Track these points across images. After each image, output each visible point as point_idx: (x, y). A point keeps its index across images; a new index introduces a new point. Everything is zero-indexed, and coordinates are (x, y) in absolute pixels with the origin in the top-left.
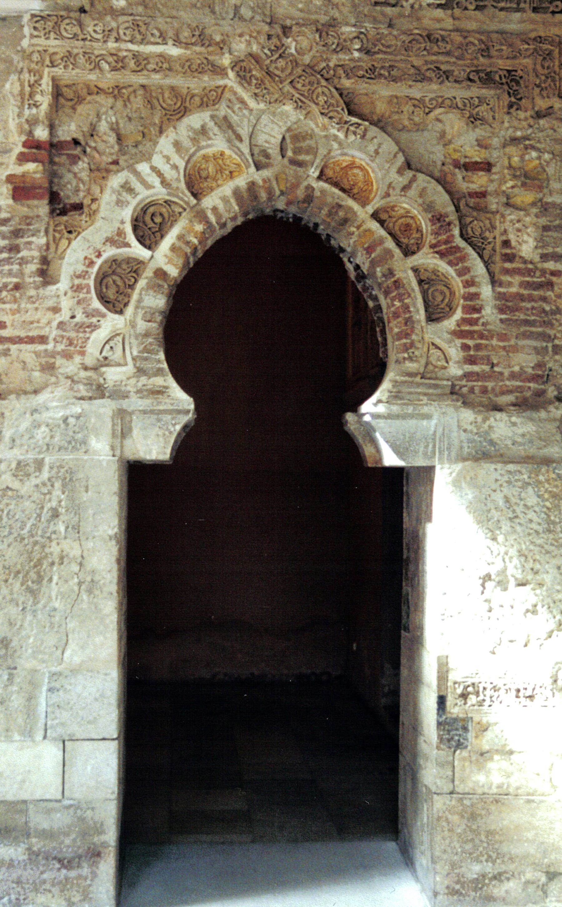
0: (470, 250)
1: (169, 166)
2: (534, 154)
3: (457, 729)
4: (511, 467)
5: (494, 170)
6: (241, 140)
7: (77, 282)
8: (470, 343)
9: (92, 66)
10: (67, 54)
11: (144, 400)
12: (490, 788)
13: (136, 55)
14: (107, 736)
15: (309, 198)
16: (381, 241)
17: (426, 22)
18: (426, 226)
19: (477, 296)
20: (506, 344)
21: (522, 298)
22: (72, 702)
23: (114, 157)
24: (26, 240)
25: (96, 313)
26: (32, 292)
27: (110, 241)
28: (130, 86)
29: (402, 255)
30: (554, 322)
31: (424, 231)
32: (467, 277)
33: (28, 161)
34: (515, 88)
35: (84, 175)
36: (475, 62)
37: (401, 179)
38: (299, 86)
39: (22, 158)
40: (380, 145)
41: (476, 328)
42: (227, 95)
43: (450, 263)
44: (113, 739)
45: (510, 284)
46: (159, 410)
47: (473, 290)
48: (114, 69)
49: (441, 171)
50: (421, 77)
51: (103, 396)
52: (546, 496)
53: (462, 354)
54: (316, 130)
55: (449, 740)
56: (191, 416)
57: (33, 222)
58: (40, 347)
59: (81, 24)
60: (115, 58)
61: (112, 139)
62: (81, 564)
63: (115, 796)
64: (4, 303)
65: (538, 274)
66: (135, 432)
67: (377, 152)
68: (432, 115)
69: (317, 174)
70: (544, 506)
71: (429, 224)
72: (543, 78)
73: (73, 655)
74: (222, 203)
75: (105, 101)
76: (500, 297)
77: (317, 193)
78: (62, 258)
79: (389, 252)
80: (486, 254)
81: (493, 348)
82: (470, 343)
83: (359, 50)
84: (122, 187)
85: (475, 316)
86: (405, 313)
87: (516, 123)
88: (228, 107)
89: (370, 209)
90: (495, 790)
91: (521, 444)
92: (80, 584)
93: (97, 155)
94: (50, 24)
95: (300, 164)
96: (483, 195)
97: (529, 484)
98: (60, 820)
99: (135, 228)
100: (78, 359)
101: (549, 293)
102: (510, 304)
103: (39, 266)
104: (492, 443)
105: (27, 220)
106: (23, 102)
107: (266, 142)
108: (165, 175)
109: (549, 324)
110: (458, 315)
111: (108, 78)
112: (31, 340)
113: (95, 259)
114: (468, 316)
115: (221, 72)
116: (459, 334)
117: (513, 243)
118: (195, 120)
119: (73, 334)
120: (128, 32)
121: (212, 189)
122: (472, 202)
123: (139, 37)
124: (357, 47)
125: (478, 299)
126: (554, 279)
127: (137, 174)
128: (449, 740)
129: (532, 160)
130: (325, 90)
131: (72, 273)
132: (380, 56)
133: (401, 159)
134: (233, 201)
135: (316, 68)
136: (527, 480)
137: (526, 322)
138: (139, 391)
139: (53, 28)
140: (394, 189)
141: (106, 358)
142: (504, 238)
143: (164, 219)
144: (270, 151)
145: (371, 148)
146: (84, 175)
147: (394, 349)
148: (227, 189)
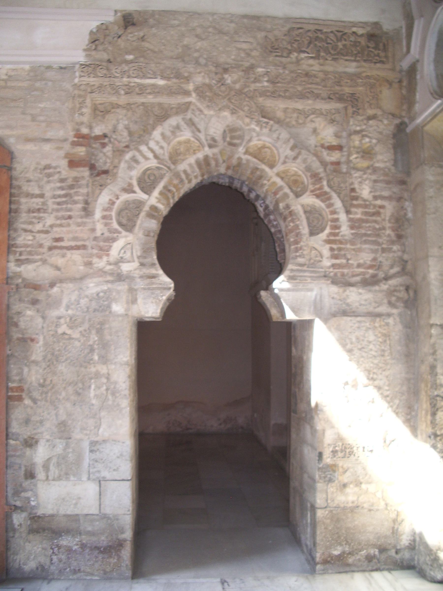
2: (367, 140)
3: (329, 471)
4: (359, 319)
8: (335, 246)
9: (114, 92)
12: (347, 503)
13: (139, 85)
14: (125, 478)
15: (239, 164)
17: (304, 67)
18: (308, 180)
19: (337, 220)
22: (104, 459)
23: (127, 144)
24: (75, 190)
25: (116, 231)
26: (79, 220)
28: (136, 103)
30: (382, 235)
31: (306, 183)
32: (331, 209)
34: (356, 103)
35: (110, 154)
36: (333, 89)
38: (233, 101)
39: (74, 144)
41: (337, 238)
42: (192, 107)
43: (323, 201)
44: (128, 480)
46: (154, 288)
47: (335, 216)
48: (126, 93)
49: (315, 150)
50: (302, 96)
52: (379, 335)
54: (243, 126)
55: (325, 477)
56: (170, 292)
59: (108, 69)
60: (128, 87)
61: (125, 134)
62: (108, 379)
63: (130, 512)
65: (372, 207)
66: (140, 301)
67: (278, 138)
68: (309, 119)
69: (244, 150)
70: (378, 341)
71: (309, 178)
72: (371, 98)
73: (104, 432)
75: (121, 112)
76: (350, 220)
77: (244, 162)
78: (96, 201)
79: (286, 196)
81: (347, 250)
82: (335, 246)
83: (267, 81)
87: (356, 122)
90: (350, 505)
91: (364, 305)
92: (107, 390)
93: (116, 142)
95: (234, 145)
97: (370, 328)
98: (98, 525)
99: (139, 184)
100: (105, 259)
101: (378, 219)
102: (357, 224)
103: (83, 205)
104: (348, 305)
105: (76, 179)
107: (215, 133)
109: (378, 235)
111: (123, 100)
114: (333, 231)
115: (187, 93)
116: (328, 242)
117: (358, 190)
118: (173, 121)
119: (102, 244)
120: (135, 72)
121: (183, 160)
123: (141, 74)
124: (266, 79)
128: (325, 477)
129: (366, 143)
132: (279, 85)
135: (243, 91)
136: (369, 326)
137: (365, 235)
138: (141, 277)
141: (122, 258)
144: (217, 138)
145: (275, 136)
147: (290, 250)
148: (192, 160)
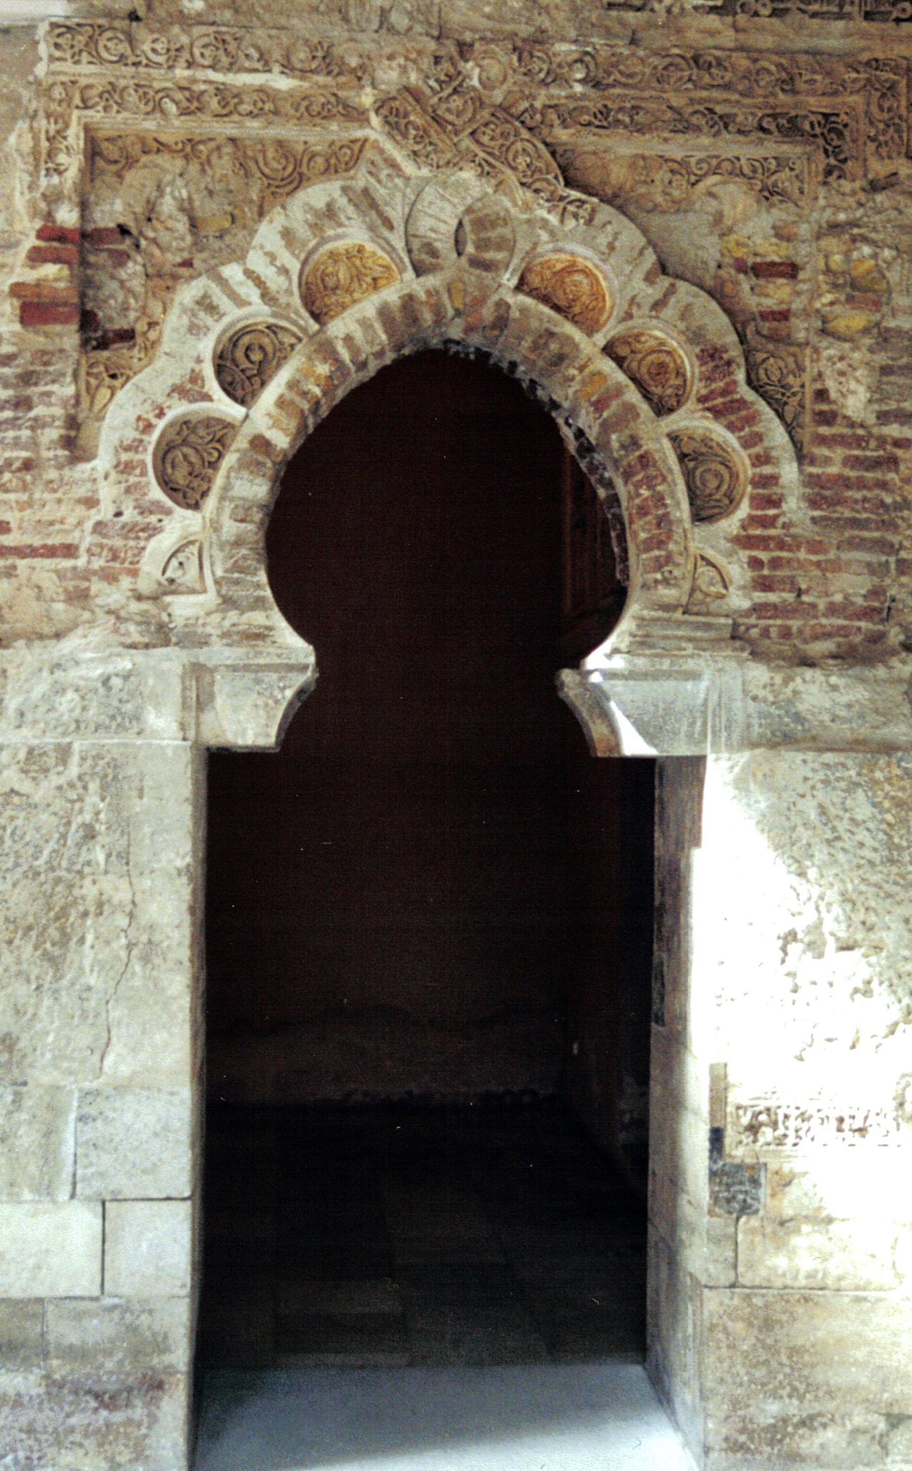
0: (762, 406)
1: (274, 269)
2: (867, 250)
3: (741, 1183)
4: (829, 757)
5: (802, 275)
6: (391, 227)
7: (125, 457)
8: (763, 556)
9: (149, 108)
10: (109, 88)
11: (234, 649)
12: (795, 1278)
13: (220, 90)
14: (174, 1194)
15: (501, 322)
16: (619, 391)
17: (692, 36)
18: (692, 366)
19: (773, 479)
20: (821, 557)
21: (847, 483)
22: (117, 1139)
23: (186, 255)
24: (42, 388)
25: (156, 508)
27: (179, 391)
28: (211, 139)
29: (652, 414)
30: (900, 522)
31: (689, 374)
32: (758, 449)
33: (45, 260)
34: (836, 142)
35: (137, 284)
36: (771, 100)
37: (650, 291)
38: (485, 139)
39: (36, 257)
40: (616, 235)
41: (772, 532)
42: (368, 154)
43: (731, 427)
44: (184, 1199)
45: (827, 461)
46: (259, 665)
47: (767, 470)
48: (185, 112)
49: (716, 277)
50: (683, 125)
51: (167, 643)
52: (887, 804)
53: (749, 574)
54: (514, 211)
56: (309, 675)
57: (54, 359)
58: (66, 564)
59: (131, 39)
60: (187, 94)
61: (182, 225)
63: (186, 1291)
64: (7, 491)
65: (873, 444)
67: (611, 247)
68: (701, 186)
69: (514, 282)
70: (883, 821)
71: (697, 363)
72: (881, 126)
73: (119, 1063)
74: (360, 328)
75: (171, 164)
76: (812, 481)
77: (515, 314)
78: (100, 418)
79: (631, 409)
80: (789, 411)
81: (801, 565)
82: (763, 556)
83: (582, 81)
84: (198, 303)
85: (772, 512)
86: (657, 507)
87: (837, 200)
88: (370, 173)
89: (600, 339)
90: (802, 1282)
91: (845, 720)
92: (130, 947)
93: (157, 252)
94: (81, 39)
95: (487, 266)
96: (784, 316)
97: (858, 785)
98: (97, 1329)
99: (219, 370)
100: (126, 582)
101: (891, 476)
102: (827, 493)
103: (63, 432)
104: (798, 718)
105: (44, 357)
106: (37, 166)
107: (432, 230)
108: (269, 284)
109: (892, 526)
110: (744, 510)
111: (176, 127)
112: (51, 552)
113: (154, 421)
114: (759, 513)
115: (358, 116)
116: (744, 541)
117: (833, 395)
118: (317, 194)
119: (118, 542)
120: (207, 52)
121: (344, 307)
122: (766, 327)
123: (225, 60)
124: (579, 76)
125: (776, 484)
126: (899, 453)
127: (223, 282)
128: (728, 1201)
129: (863, 259)
130: (528, 146)
131: (117, 443)
132: (617, 91)
133: (650, 258)
134: (378, 326)
135: (513, 110)
136: (855, 779)
137: (854, 523)
138: (225, 635)
139: (87, 45)
140: (639, 306)
141: (172, 581)
142: (818, 386)
143: (266, 354)
144: (438, 245)
145: (603, 240)
146: (137, 284)
147: (639, 566)
148: (368, 307)
